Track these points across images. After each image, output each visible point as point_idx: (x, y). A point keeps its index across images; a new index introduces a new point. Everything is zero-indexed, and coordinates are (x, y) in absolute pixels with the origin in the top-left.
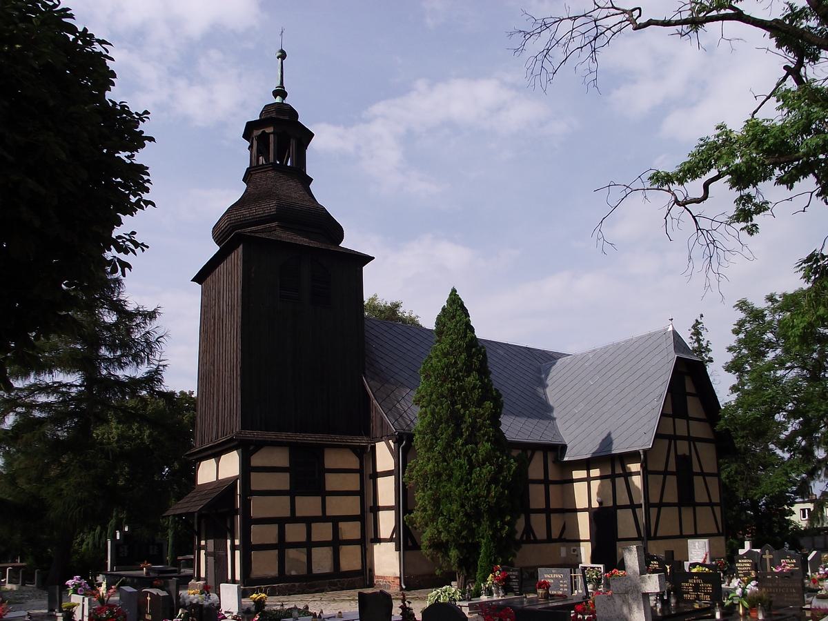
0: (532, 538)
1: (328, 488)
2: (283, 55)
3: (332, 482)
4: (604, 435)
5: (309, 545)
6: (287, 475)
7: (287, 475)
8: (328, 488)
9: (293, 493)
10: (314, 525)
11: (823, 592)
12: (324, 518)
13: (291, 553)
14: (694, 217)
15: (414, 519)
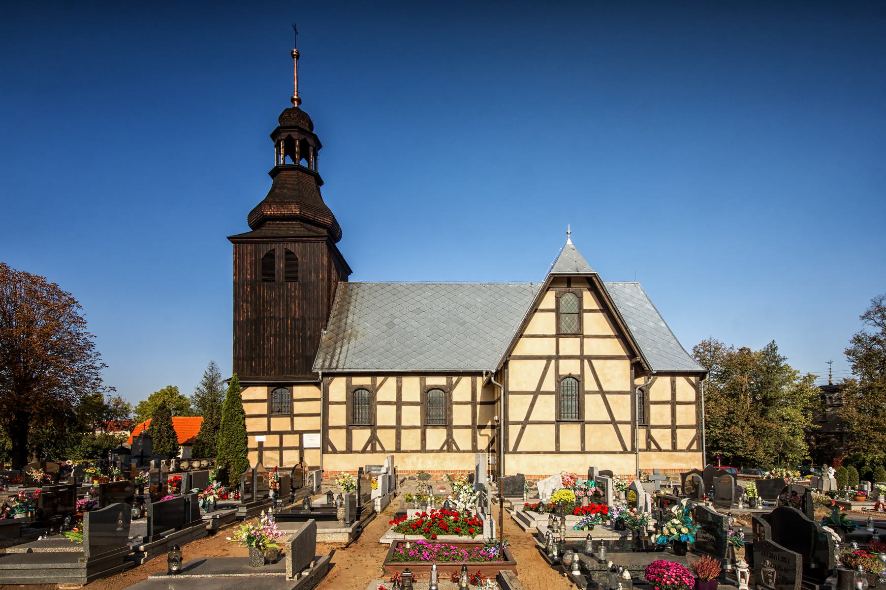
0: (454, 448)
1: (295, 412)
3: (298, 408)
4: (770, 342)
5: (281, 449)
6: (330, 400)
7: (330, 400)
8: (295, 412)
9: (269, 416)
10: (284, 436)
11: (2, 480)
12: (293, 432)
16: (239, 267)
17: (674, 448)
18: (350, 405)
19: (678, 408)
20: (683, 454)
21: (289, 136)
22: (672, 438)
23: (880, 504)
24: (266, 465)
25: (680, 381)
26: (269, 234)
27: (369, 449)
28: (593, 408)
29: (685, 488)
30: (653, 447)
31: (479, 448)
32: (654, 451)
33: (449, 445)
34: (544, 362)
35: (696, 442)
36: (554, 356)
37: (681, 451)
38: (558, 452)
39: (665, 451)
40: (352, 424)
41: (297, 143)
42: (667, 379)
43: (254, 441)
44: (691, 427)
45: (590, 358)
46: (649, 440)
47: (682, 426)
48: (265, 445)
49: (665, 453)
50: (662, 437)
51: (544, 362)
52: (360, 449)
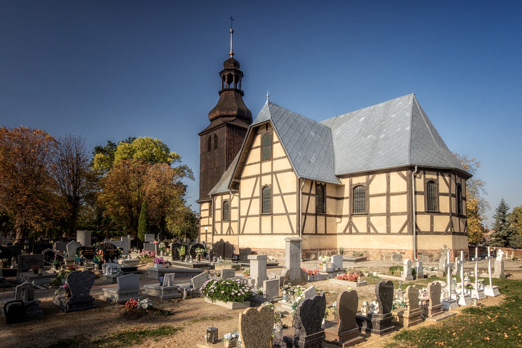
17: (389, 232)
18: (222, 209)
19: (392, 198)
20: (395, 237)
21: (230, 73)
22: (387, 223)
23: (501, 293)
25: (394, 176)
27: (348, 231)
28: (277, 205)
29: (180, 255)
30: (372, 231)
31: (223, 233)
32: (373, 234)
33: (370, 230)
34: (255, 179)
35: (407, 226)
36: (259, 174)
37: (394, 234)
38: (261, 234)
39: (381, 234)
40: (353, 214)
41: (234, 76)
42: (384, 176)
44: (403, 214)
45: (276, 173)
46: (369, 226)
47: (395, 213)
48: (208, 232)
49: (381, 236)
50: (379, 223)
51: (255, 179)
52: (397, 231)
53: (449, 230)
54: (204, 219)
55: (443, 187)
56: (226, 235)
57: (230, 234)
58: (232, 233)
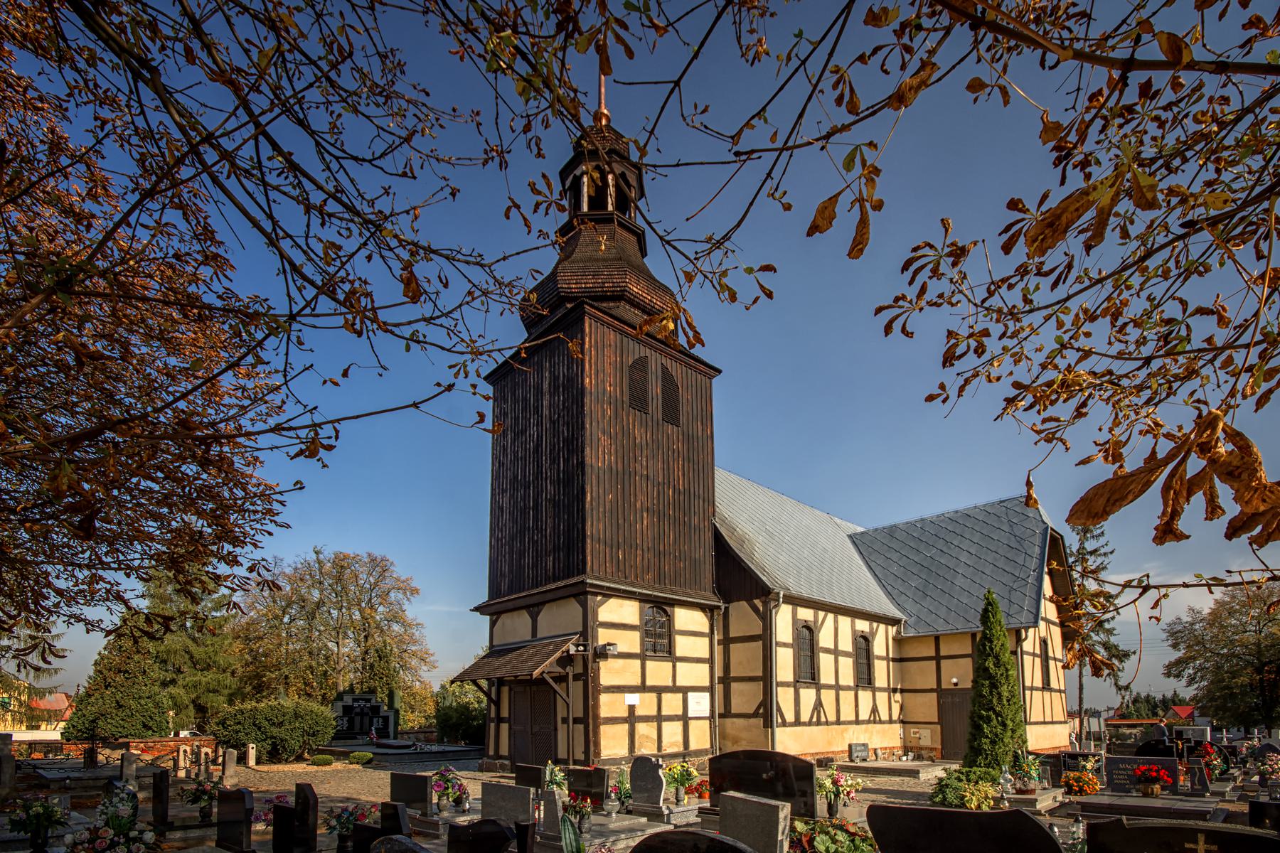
2: (687, 220)
5: (659, 719)
12: (674, 689)
13: (641, 728)
14: (286, 363)
15: (1095, 725)
16: (596, 364)
18: (590, 623)
24: (640, 750)
26: (614, 312)
43: (609, 705)
53: (761, 711)
54: (621, 662)
55: (879, 647)
56: (810, 723)
57: (819, 723)
58: (823, 719)
